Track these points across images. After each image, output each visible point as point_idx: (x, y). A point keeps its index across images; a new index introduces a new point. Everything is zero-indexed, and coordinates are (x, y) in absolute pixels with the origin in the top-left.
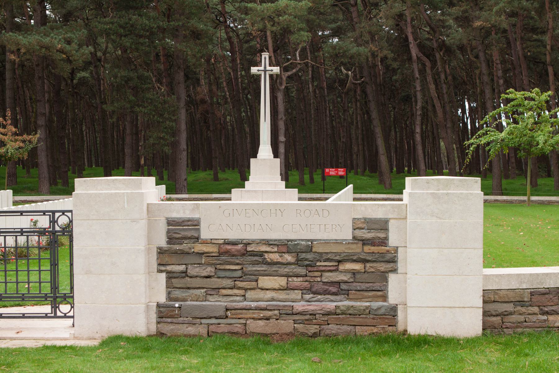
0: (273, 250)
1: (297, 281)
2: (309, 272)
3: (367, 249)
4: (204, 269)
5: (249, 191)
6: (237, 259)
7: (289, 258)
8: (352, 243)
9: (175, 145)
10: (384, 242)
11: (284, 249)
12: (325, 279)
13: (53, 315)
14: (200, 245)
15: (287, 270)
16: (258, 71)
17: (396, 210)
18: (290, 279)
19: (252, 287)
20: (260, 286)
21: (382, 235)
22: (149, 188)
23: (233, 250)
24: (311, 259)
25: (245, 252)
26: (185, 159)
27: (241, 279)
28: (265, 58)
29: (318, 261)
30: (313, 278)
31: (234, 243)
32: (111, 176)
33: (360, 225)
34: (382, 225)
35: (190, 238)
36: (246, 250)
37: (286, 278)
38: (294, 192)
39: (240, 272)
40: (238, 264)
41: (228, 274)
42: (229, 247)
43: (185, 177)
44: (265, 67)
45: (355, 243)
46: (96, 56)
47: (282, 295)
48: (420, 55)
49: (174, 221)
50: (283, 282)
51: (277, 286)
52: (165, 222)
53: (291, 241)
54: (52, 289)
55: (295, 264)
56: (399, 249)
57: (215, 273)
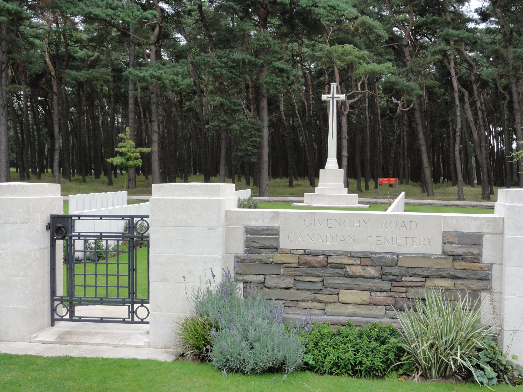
0: (355, 263)
1: (380, 297)
2: (394, 287)
3: (458, 264)
4: (283, 280)
5: (318, 195)
6: (318, 270)
7: (372, 271)
8: (441, 258)
9: (260, 156)
10: (477, 258)
11: (368, 262)
12: (411, 295)
13: (130, 320)
14: (279, 255)
15: (369, 284)
16: (328, 97)
17: (491, 224)
18: (373, 294)
19: (332, 301)
20: (340, 300)
21: (475, 251)
22: (227, 195)
23: (313, 261)
24: (397, 274)
25: (326, 264)
26: (267, 169)
27: (321, 292)
28: (333, 87)
29: (403, 276)
30: (398, 294)
31: (315, 254)
32: (210, 182)
33: (451, 240)
34: (476, 240)
35: (268, 248)
36: (327, 262)
37: (369, 292)
38: (355, 197)
39: (321, 284)
40: (318, 276)
41: (307, 286)
42: (309, 258)
43: (267, 183)
44: (333, 95)
45: (444, 258)
46: (200, 88)
47: (364, 311)
48: (460, 86)
49: (252, 230)
50: (365, 296)
51: (359, 301)
52: (243, 230)
53: (376, 253)
54: (129, 294)
55: (379, 278)
56: (494, 266)
57: (295, 284)
